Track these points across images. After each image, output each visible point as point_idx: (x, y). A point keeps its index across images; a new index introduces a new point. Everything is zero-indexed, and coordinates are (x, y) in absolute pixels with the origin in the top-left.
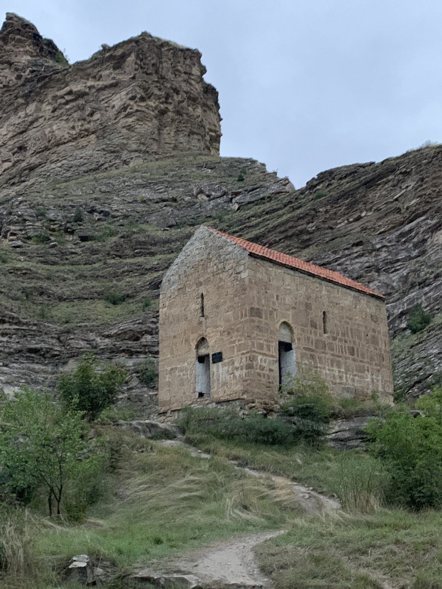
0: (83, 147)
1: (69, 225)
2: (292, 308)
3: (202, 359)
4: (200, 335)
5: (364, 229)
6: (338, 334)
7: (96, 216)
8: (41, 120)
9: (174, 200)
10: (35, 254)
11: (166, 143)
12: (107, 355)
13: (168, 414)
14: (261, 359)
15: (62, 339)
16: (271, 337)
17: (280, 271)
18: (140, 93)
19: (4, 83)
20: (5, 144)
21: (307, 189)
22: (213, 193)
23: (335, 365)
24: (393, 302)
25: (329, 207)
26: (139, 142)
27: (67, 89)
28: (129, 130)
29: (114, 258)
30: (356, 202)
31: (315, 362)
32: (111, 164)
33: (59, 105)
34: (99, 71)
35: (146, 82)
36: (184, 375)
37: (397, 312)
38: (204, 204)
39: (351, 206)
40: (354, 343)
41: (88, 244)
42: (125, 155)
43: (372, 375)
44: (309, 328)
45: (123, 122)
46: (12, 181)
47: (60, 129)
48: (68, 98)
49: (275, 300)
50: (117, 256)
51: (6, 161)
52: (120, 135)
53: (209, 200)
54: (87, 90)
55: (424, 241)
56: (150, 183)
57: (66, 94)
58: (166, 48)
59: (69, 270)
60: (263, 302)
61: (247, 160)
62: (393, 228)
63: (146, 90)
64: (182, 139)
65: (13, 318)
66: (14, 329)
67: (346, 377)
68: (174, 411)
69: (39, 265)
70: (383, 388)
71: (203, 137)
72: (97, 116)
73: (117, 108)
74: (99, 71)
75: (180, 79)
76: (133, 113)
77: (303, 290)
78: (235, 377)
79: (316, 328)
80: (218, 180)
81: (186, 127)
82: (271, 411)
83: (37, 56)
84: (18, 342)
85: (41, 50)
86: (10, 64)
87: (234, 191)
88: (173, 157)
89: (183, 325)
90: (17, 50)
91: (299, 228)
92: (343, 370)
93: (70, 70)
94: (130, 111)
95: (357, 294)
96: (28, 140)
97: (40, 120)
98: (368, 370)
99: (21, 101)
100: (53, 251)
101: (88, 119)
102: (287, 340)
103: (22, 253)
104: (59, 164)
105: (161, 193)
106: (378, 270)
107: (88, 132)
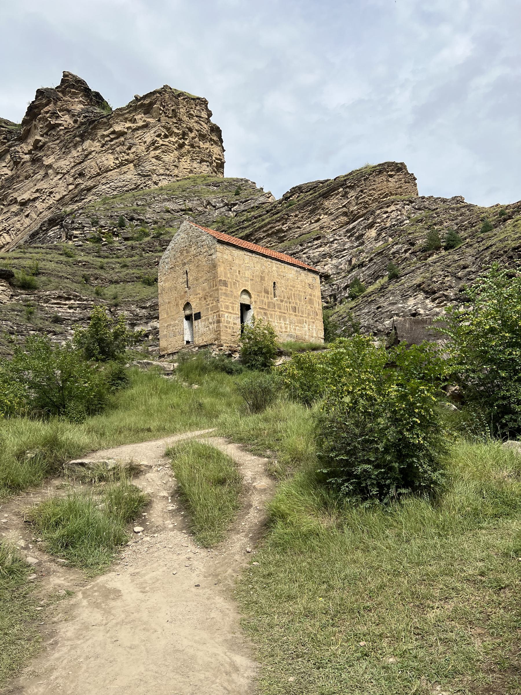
0: (125, 173)
1: (115, 229)
2: (251, 280)
3: (188, 318)
4: (186, 301)
5: (322, 228)
6: (284, 297)
7: (135, 223)
8: (93, 153)
9: (190, 210)
10: (92, 251)
11: (185, 169)
12: (145, 320)
13: (166, 357)
14: (227, 317)
15: (112, 310)
16: (235, 301)
17: (241, 253)
18: (164, 132)
19: (65, 126)
20: (69, 172)
21: (283, 200)
22: (218, 205)
23: (282, 319)
24: (341, 279)
25: (297, 213)
26: (164, 168)
27: (112, 129)
28: (157, 159)
29: (148, 252)
30: (317, 208)
31: (268, 317)
32: (145, 185)
33: (106, 142)
34: (134, 116)
35: (169, 123)
36: (176, 329)
37: (343, 285)
38: (211, 213)
39: (312, 212)
40: (296, 303)
41: (129, 243)
42: (155, 178)
43: (309, 325)
44: (263, 294)
45: (152, 153)
46: (76, 199)
47: (109, 160)
48: (112, 136)
49: (238, 274)
50: (150, 251)
51: (70, 184)
52: (151, 163)
53: (215, 210)
54: (126, 130)
55: (363, 235)
56: (173, 198)
57: (111, 134)
58: (182, 98)
59: (116, 262)
60: (229, 275)
61: (242, 180)
62: (341, 227)
63: (168, 129)
64: (195, 165)
65: (76, 296)
66: (78, 304)
67: (290, 328)
68: (170, 354)
69: (95, 258)
70: (317, 334)
71: (211, 163)
72: (133, 150)
73: (147, 143)
74: (134, 116)
75: (193, 121)
76: (159, 146)
77: (258, 267)
78: (210, 329)
79: (268, 294)
80: (221, 195)
81: (198, 156)
82: (235, 351)
83: (88, 104)
84: (81, 313)
85: (91, 100)
86: (69, 111)
87: (232, 202)
88: (189, 178)
89: (175, 294)
90: (73, 100)
91: (277, 228)
92: (288, 323)
93: (113, 115)
94: (157, 145)
95: (299, 269)
96: (85, 168)
97: (93, 153)
98: (306, 322)
99: (78, 139)
100: (105, 248)
101: (127, 151)
102: (247, 302)
103: (82, 250)
104: (108, 186)
105: (180, 205)
106: (331, 257)
107: (129, 162)
